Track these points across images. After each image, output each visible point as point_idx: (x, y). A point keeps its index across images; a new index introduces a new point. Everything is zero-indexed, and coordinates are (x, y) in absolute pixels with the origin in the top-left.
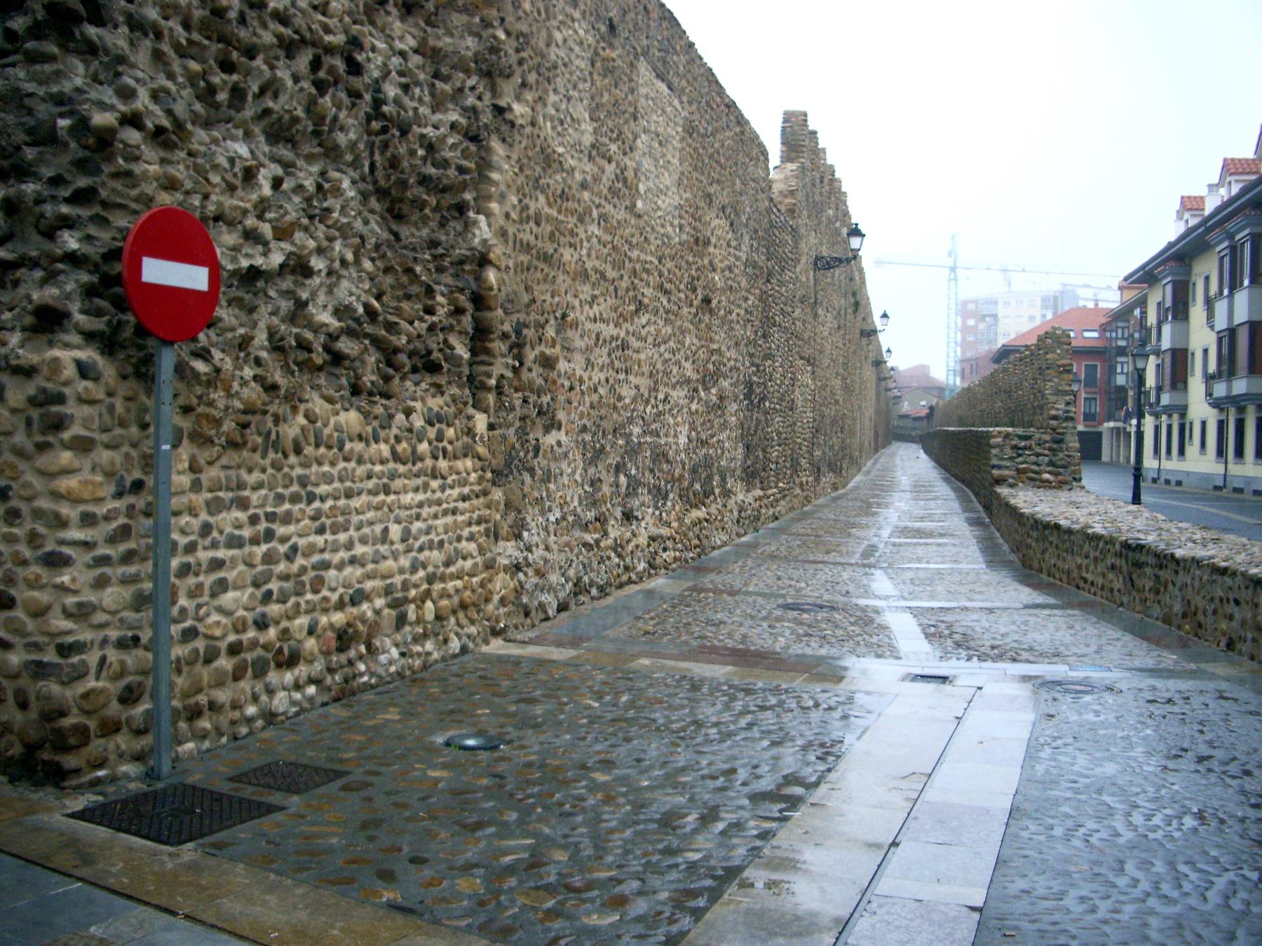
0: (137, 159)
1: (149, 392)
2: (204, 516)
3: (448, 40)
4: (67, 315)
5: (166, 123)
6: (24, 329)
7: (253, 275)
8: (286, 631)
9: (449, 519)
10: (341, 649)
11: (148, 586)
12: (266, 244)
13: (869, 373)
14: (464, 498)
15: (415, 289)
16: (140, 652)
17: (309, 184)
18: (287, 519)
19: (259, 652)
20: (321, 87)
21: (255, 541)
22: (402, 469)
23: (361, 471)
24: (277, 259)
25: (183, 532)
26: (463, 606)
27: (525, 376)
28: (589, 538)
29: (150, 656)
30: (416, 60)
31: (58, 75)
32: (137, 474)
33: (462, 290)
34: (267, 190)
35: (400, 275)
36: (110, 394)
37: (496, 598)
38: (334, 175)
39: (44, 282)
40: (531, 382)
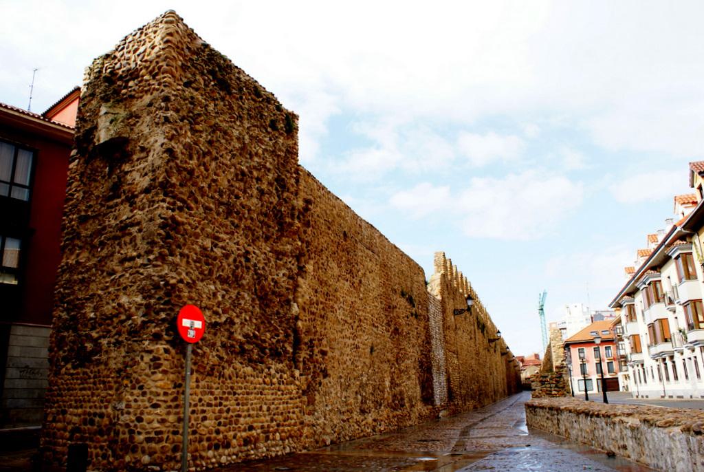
0: (181, 291)
2: (200, 396)
3: (281, 247)
5: (190, 281)
7: (216, 323)
9: (285, 405)
12: (220, 315)
14: (291, 399)
15: (271, 329)
16: (179, 436)
18: (227, 399)
19: (216, 441)
20: (237, 267)
21: (216, 406)
22: (267, 387)
23: (252, 386)
24: (223, 319)
27: (315, 357)
28: (345, 418)
30: (271, 254)
32: (180, 382)
33: (289, 329)
35: (265, 319)
36: (173, 358)
37: (304, 435)
38: (242, 293)
39: (155, 327)
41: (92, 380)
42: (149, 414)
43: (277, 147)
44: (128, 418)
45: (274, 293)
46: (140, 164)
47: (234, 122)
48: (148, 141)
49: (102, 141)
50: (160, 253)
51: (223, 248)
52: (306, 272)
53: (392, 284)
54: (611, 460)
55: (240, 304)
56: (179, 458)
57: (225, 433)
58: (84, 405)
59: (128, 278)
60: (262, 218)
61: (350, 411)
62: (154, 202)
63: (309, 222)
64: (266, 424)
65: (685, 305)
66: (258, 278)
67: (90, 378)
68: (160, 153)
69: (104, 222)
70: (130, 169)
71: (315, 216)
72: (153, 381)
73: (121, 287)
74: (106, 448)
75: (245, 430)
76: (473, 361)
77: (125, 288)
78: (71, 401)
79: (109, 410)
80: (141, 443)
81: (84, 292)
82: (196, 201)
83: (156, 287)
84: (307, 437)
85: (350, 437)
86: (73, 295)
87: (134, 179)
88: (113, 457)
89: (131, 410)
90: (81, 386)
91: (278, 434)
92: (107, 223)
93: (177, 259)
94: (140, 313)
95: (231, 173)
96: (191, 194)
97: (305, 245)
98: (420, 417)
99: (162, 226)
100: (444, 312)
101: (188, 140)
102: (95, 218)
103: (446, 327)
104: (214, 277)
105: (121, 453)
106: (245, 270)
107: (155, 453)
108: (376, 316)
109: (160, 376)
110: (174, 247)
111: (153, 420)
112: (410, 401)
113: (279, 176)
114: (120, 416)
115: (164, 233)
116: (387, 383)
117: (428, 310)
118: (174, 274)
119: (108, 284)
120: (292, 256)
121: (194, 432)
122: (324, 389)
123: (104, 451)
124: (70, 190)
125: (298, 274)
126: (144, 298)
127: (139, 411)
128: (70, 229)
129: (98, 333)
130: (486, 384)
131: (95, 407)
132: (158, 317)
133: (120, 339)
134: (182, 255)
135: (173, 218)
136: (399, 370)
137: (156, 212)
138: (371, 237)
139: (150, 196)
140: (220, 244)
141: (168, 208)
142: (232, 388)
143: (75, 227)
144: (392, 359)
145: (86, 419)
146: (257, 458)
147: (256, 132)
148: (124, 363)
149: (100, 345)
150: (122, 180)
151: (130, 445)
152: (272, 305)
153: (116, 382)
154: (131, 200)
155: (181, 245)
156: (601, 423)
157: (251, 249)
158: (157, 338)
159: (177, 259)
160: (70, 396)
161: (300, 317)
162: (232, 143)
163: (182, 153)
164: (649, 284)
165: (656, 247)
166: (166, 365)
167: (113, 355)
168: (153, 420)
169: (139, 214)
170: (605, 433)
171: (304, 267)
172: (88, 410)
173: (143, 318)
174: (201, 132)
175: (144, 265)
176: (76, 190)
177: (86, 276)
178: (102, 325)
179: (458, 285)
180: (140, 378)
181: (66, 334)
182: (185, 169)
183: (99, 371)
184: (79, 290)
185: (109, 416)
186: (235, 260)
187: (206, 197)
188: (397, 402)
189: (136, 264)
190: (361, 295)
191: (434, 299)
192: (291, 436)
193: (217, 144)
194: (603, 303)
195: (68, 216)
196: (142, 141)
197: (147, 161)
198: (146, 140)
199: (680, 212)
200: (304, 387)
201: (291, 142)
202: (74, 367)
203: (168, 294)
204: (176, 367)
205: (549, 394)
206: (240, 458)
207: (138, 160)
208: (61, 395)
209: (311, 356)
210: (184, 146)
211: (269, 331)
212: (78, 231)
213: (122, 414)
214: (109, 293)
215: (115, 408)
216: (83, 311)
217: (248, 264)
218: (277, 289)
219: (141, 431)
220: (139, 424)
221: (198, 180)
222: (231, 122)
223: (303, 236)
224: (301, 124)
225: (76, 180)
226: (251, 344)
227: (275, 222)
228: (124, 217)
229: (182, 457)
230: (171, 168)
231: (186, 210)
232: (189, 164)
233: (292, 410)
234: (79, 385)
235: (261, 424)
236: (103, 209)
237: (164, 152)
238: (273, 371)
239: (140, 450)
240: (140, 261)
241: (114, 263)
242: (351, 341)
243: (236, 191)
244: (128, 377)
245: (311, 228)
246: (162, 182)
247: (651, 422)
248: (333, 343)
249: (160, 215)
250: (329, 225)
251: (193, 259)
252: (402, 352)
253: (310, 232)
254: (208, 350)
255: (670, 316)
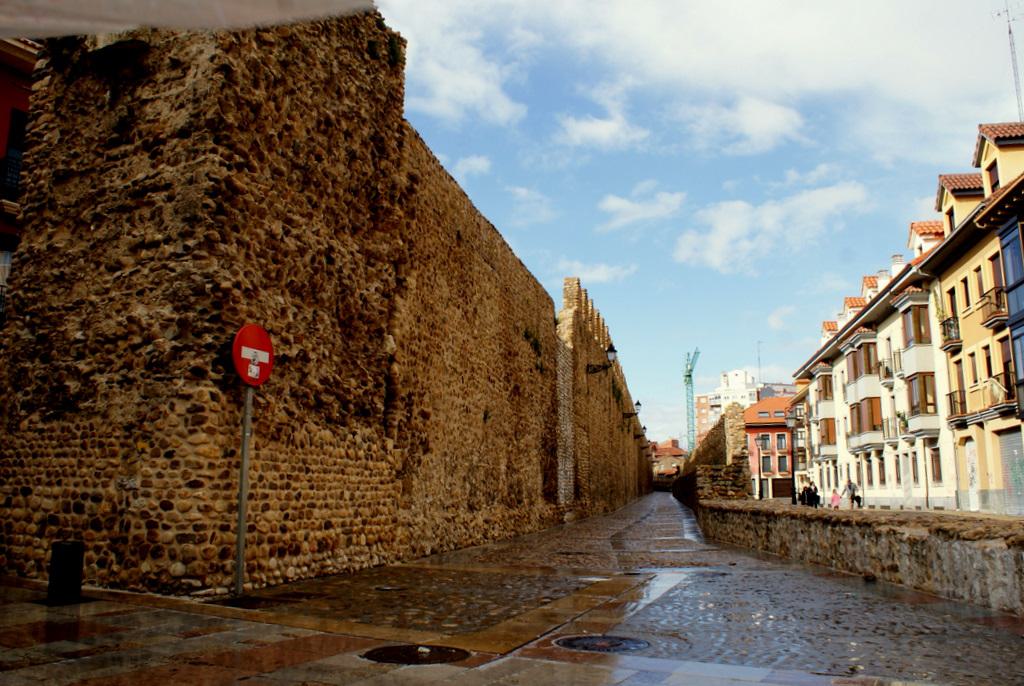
0: (238, 302)
1: (239, 410)
2: (260, 472)
3: (373, 245)
4: (206, 372)
5: (250, 287)
6: (186, 378)
7: (285, 358)
8: (294, 536)
9: (374, 492)
10: (319, 551)
11: (235, 502)
12: (290, 344)
13: (630, 441)
14: (382, 483)
15: (357, 373)
16: (230, 533)
17: (309, 317)
18: (297, 479)
19: (281, 544)
20: (316, 271)
21: (282, 488)
22: (351, 462)
23: (331, 461)
24: (294, 352)
25: (251, 478)
26: (380, 540)
27: (413, 422)
28: (450, 516)
29: (235, 536)
30: (359, 256)
31: (207, 265)
32: (233, 448)
33: (380, 375)
34: (291, 319)
35: (348, 360)
36: (223, 409)
37: (398, 539)
38: (321, 313)
39: (195, 357)
40: (416, 425)
41: (78, 441)
42: (182, 497)
43: (377, 86)
44: (145, 503)
45: (361, 317)
46: (170, 88)
47: (318, 36)
48: (187, 50)
49: (101, 45)
50: (206, 237)
51: (298, 237)
52: (406, 288)
53: (514, 318)
54: (871, 586)
55: (318, 330)
56: (229, 568)
57: (294, 532)
58: (65, 480)
59: (147, 276)
60: (350, 197)
61: (456, 506)
62: (197, 152)
63: (413, 210)
64: (348, 520)
65: (909, 380)
66: (343, 291)
67: (75, 437)
68: (209, 72)
69: (102, 182)
70: (151, 96)
71: (422, 203)
72: (191, 444)
73: (134, 291)
74: (105, 549)
75: (320, 528)
76: (606, 443)
77: (141, 293)
78: (40, 473)
79: (112, 490)
80: (169, 543)
81: (62, 298)
82: (261, 158)
83: (199, 292)
84: (401, 542)
85: (456, 545)
86: (43, 301)
87: (159, 114)
88: (119, 563)
89: (152, 491)
90: (59, 450)
91: (363, 536)
92: (107, 184)
93: (232, 249)
94: (170, 333)
95: (312, 118)
96: (255, 145)
97: (407, 246)
98: (542, 519)
99: (212, 193)
100: (575, 367)
101: (253, 55)
102: (83, 174)
103: (576, 391)
104: (283, 283)
105: (133, 559)
106: (327, 277)
107: (194, 559)
108: (493, 365)
109: (203, 436)
110: (228, 229)
111: (191, 508)
112: (530, 496)
113: (376, 133)
114: (131, 499)
115: (213, 205)
116: (503, 468)
117: (556, 363)
118: (227, 274)
119: (108, 286)
120: (389, 262)
121: (252, 529)
122: (424, 470)
123: (102, 555)
124: (34, 127)
125: (394, 291)
126: (176, 309)
127: (165, 493)
128: (35, 192)
129: (90, 363)
130: (618, 477)
131: (85, 483)
132: (199, 341)
133: (131, 375)
134: (240, 242)
135: (228, 181)
136: (518, 448)
137: (201, 169)
138: (491, 245)
139: (189, 142)
140: (295, 232)
141: (221, 164)
142: (304, 462)
143: (45, 190)
144: (510, 432)
145: (69, 503)
146: (335, 571)
147: (347, 57)
148: (139, 414)
149: (94, 385)
150: (136, 113)
151: (148, 546)
152: (358, 335)
153: (122, 445)
154: (153, 147)
155: (240, 226)
156: (852, 534)
157: (334, 243)
158: (198, 374)
159: (232, 249)
160: (39, 465)
161: (397, 358)
162: (315, 70)
163: (244, 76)
164: (859, 347)
165: (874, 296)
166: (212, 420)
167: (118, 400)
168: (191, 508)
169: (168, 172)
170: (858, 548)
171: (405, 280)
172: (71, 488)
173: (174, 343)
174: (271, 44)
175: (176, 256)
176: (46, 128)
177: (67, 270)
178: (99, 351)
179: (593, 328)
180: (167, 439)
181: (28, 365)
182: (249, 103)
183: (92, 427)
184: (54, 293)
185: (110, 499)
186: (313, 260)
187: (274, 154)
188: (513, 496)
189: (162, 253)
190: (476, 332)
191: (564, 348)
192: (380, 540)
193: (293, 68)
194: (783, 373)
195: (31, 171)
196: (174, 51)
197: (183, 84)
198: (181, 49)
199: (917, 245)
200: (399, 466)
201: (394, 82)
202: (45, 420)
203: (217, 305)
204: (227, 423)
205: (724, 495)
206: (313, 570)
207: (165, 81)
208: (22, 464)
209: (409, 419)
210: (247, 63)
211: (353, 376)
212: (50, 195)
213: (135, 496)
214: (111, 299)
215: (121, 486)
216: (63, 329)
217: (332, 268)
218: (366, 312)
219: (169, 523)
220: (165, 514)
221: (266, 123)
222: (314, 35)
223: (406, 233)
224: (410, 53)
225: (47, 111)
226: (332, 394)
227: (367, 205)
228: (141, 176)
229: (235, 567)
230: (226, 97)
231: (246, 170)
232: (254, 94)
233: (382, 501)
234: (54, 448)
235: (341, 520)
236: (99, 160)
237: (216, 71)
238: (358, 439)
239: (166, 554)
240: (169, 249)
241: (120, 251)
242: (459, 401)
243: (318, 148)
244: (145, 437)
245: (415, 221)
246: (212, 120)
247: (951, 533)
248: (437, 401)
249: (207, 175)
250: (440, 217)
251: (255, 251)
252: (523, 422)
253: (414, 227)
254: (272, 400)
255: (885, 394)
